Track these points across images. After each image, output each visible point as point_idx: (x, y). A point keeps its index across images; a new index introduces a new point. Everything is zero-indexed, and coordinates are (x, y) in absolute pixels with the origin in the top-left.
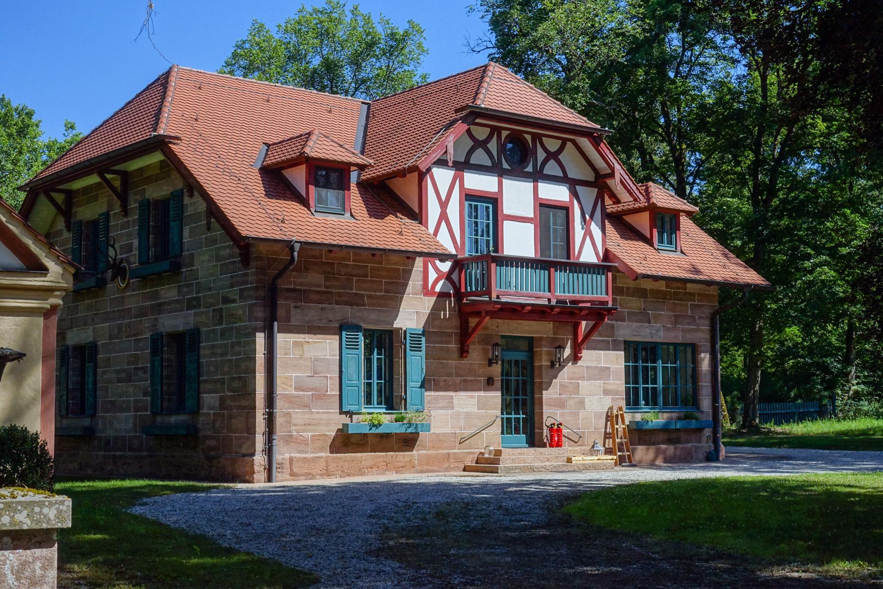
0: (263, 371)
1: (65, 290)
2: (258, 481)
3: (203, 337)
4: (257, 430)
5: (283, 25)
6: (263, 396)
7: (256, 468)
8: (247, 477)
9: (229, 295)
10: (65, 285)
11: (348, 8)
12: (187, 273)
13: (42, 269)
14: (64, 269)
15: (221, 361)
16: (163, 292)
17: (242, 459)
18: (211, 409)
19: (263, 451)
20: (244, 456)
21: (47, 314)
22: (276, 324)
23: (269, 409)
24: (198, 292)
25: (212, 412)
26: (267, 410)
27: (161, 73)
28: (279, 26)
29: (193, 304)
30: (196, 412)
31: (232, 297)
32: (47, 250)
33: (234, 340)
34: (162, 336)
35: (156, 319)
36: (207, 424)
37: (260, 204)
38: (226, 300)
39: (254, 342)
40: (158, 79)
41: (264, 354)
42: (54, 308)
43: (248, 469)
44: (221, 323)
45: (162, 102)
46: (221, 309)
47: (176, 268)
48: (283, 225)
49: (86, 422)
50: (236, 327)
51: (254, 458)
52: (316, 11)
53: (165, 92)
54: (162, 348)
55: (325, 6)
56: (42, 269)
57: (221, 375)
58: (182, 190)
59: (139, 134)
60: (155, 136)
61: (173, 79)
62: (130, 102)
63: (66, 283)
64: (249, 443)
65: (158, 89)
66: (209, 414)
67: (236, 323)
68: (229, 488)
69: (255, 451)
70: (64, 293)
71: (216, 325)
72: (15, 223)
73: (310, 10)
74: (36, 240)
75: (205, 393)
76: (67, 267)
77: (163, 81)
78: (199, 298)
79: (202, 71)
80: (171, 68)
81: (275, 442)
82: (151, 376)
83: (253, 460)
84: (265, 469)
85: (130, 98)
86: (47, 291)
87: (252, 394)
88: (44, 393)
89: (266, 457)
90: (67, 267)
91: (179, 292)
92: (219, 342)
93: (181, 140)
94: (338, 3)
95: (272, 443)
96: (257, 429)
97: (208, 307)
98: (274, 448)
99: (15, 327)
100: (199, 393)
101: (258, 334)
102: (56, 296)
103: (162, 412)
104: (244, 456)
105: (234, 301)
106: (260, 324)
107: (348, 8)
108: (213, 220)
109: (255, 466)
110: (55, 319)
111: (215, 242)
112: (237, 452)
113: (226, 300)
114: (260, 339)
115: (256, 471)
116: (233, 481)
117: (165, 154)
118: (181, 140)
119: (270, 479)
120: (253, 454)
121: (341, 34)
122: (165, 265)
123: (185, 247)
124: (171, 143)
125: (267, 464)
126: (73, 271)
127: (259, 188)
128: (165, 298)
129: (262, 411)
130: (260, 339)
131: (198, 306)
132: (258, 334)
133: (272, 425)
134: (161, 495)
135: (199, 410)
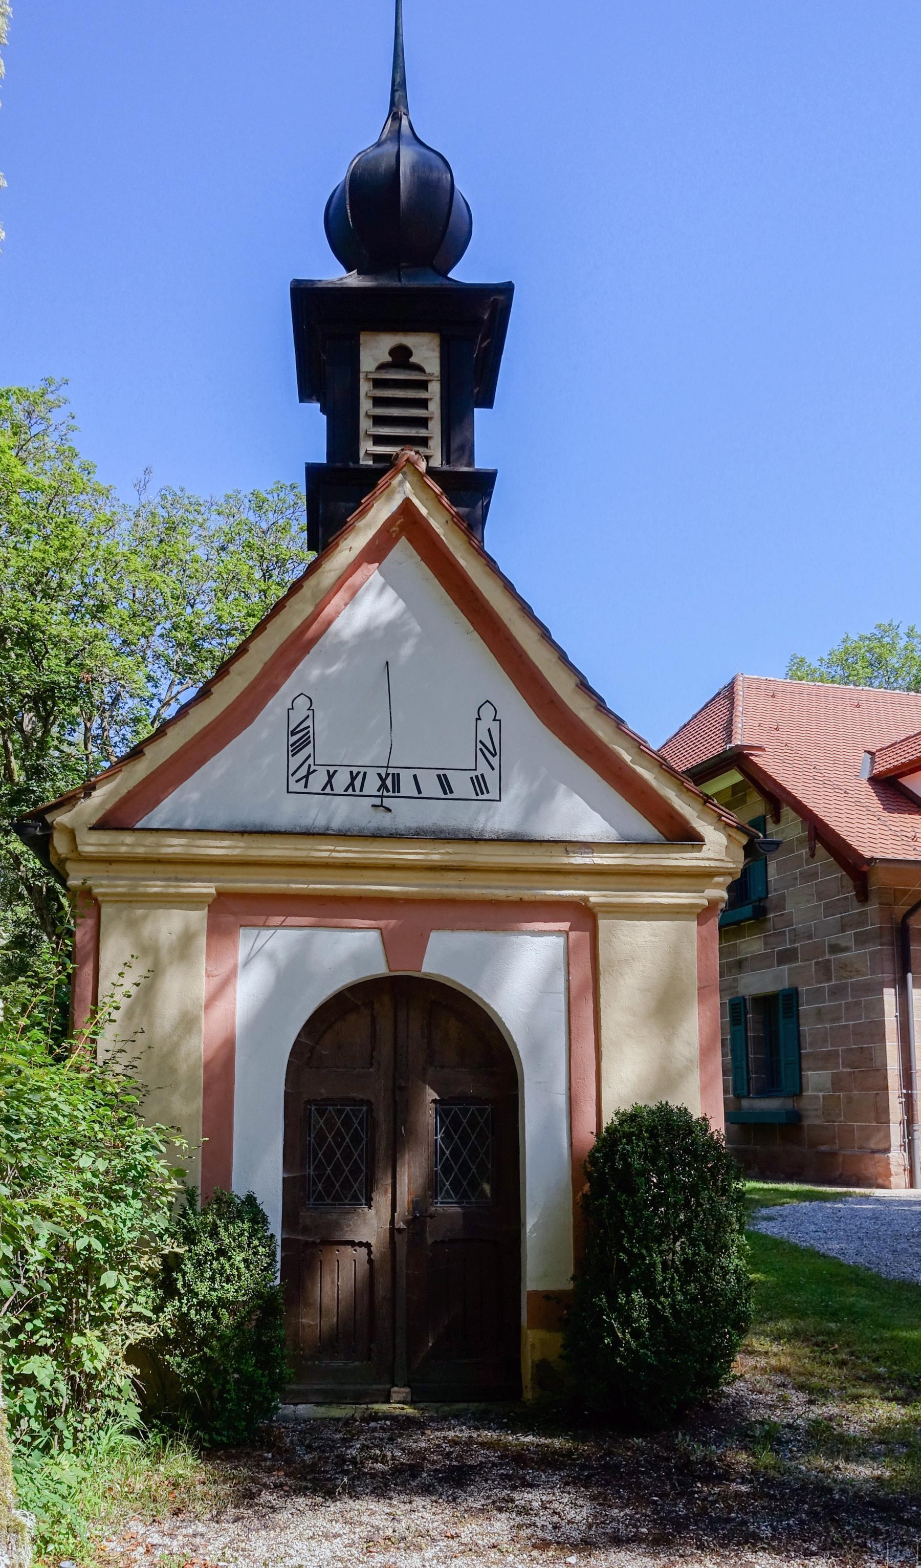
0: (896, 1039)
1: (730, 874)
2: (897, 1187)
3: (803, 998)
4: (891, 1117)
5: (826, 657)
6: (897, 1072)
7: (893, 1169)
8: (880, 1181)
9: (839, 942)
10: (731, 865)
11: (902, 631)
12: (776, 919)
13: (692, 838)
14: (729, 836)
15: (831, 1028)
16: (743, 946)
17: (870, 1155)
18: (820, 1091)
19: (901, 1146)
20: (874, 1152)
21: (702, 915)
22: (910, 976)
23: (907, 1090)
24: (793, 941)
25: (821, 1094)
26: (904, 1091)
27: (722, 687)
28: (821, 660)
29: (786, 957)
30: (798, 1092)
31: (843, 944)
32: (700, 807)
33: (850, 1000)
34: (745, 1000)
35: (736, 980)
36: (817, 1110)
37: (879, 819)
38: (835, 949)
39: (881, 1001)
40: (719, 694)
41: (896, 1016)
42: (713, 904)
43: (880, 1170)
44: (830, 979)
45: (731, 714)
46: (829, 961)
47: (760, 914)
48: (916, 843)
49: (789, 1104)
50: (851, 983)
51: (890, 1155)
52: (862, 639)
53: (732, 703)
54: (746, 1014)
55: (875, 631)
56: (692, 838)
57: (832, 1046)
58: (764, 817)
59: (712, 749)
60: (731, 748)
61: (739, 689)
62: (685, 726)
63: (734, 863)
64: (881, 1134)
65: (721, 707)
66: (818, 1097)
67: (852, 978)
68: (867, 1197)
69: (890, 1145)
70: (729, 880)
71: (821, 983)
72: (646, 763)
73: (856, 639)
74: (681, 790)
75: (809, 1069)
76: (734, 835)
77: (729, 693)
78: (796, 949)
79: (772, 679)
80: (734, 679)
81: (916, 1135)
82: (732, 1050)
83: (888, 1158)
84: (905, 1170)
85: (686, 721)
86: (703, 875)
87: (882, 1071)
88: (705, 1053)
89: (906, 1155)
90: (734, 835)
91: (765, 944)
92: (827, 1004)
93: (764, 750)
94: (890, 625)
95: (912, 1136)
96: (892, 1117)
97: (808, 960)
98: (916, 1142)
99: (653, 939)
100: (801, 1070)
101: (885, 990)
102: (718, 886)
103: (749, 1093)
104: (874, 1152)
105: (846, 949)
106: (888, 977)
107: (902, 631)
108: (819, 845)
109: (891, 1167)
110: (714, 923)
111: (812, 875)
112: (861, 1148)
113: (835, 949)
114: (890, 996)
115: (893, 1172)
116: (858, 1185)
117: (743, 771)
118: (764, 750)
119: (912, 1185)
120: (887, 1150)
121: (894, 661)
122: (747, 910)
123: (772, 887)
124: (752, 755)
125: (907, 1162)
126: (744, 841)
127: (876, 803)
128: (747, 953)
129: (898, 1093)
130: (890, 996)
131: (795, 959)
132: (885, 990)
133: (912, 1108)
134: (782, 1204)
135: (801, 1091)
